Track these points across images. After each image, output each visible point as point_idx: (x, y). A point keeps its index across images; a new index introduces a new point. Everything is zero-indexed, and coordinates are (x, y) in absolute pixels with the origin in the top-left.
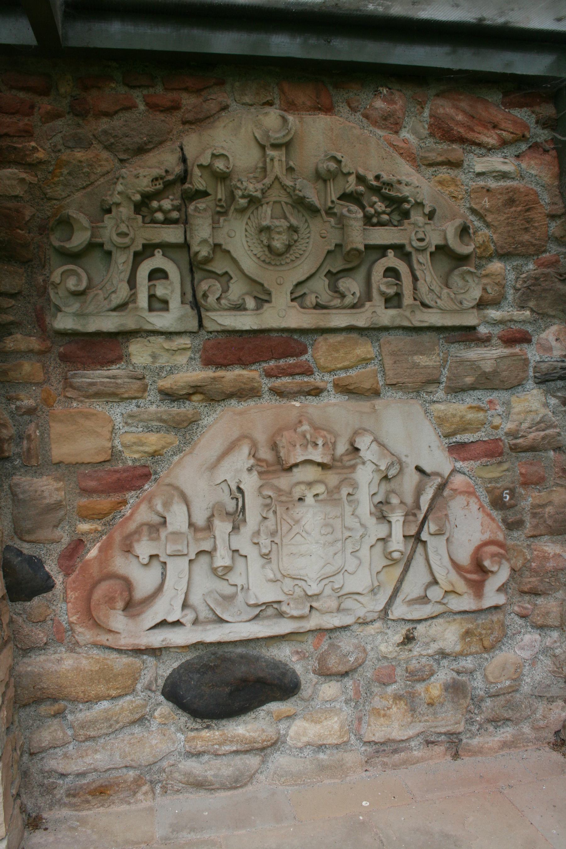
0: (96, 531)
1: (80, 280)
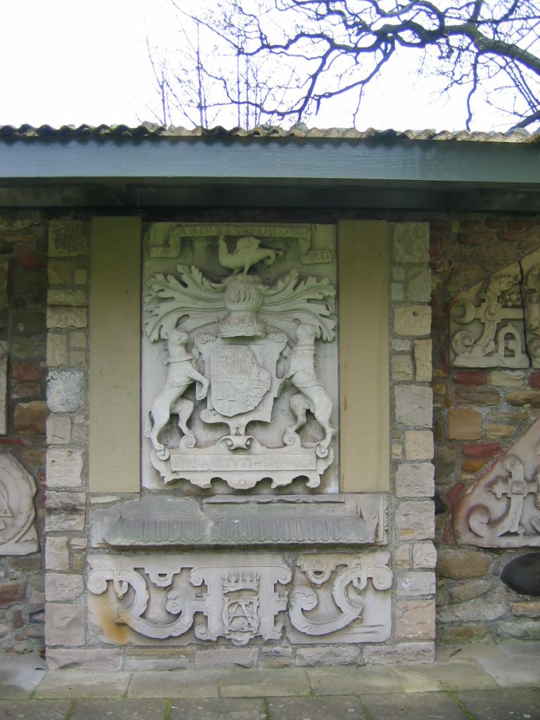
0: (471, 479)
1: (471, 341)
